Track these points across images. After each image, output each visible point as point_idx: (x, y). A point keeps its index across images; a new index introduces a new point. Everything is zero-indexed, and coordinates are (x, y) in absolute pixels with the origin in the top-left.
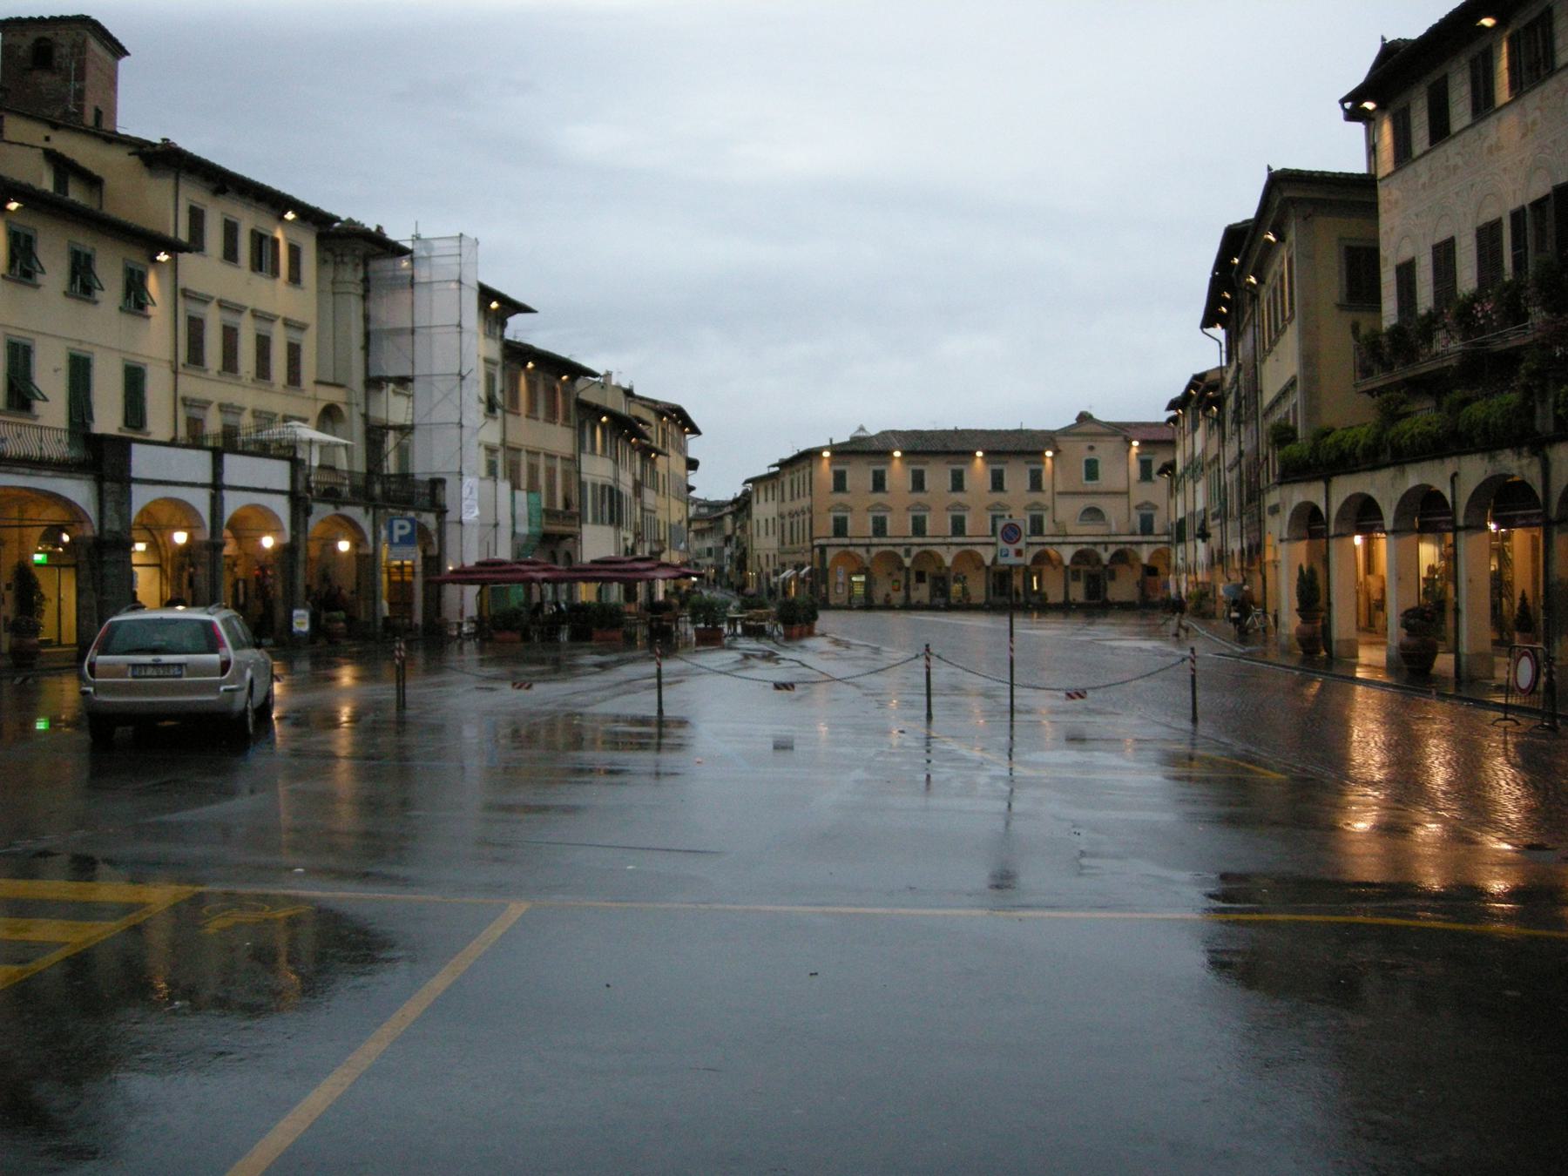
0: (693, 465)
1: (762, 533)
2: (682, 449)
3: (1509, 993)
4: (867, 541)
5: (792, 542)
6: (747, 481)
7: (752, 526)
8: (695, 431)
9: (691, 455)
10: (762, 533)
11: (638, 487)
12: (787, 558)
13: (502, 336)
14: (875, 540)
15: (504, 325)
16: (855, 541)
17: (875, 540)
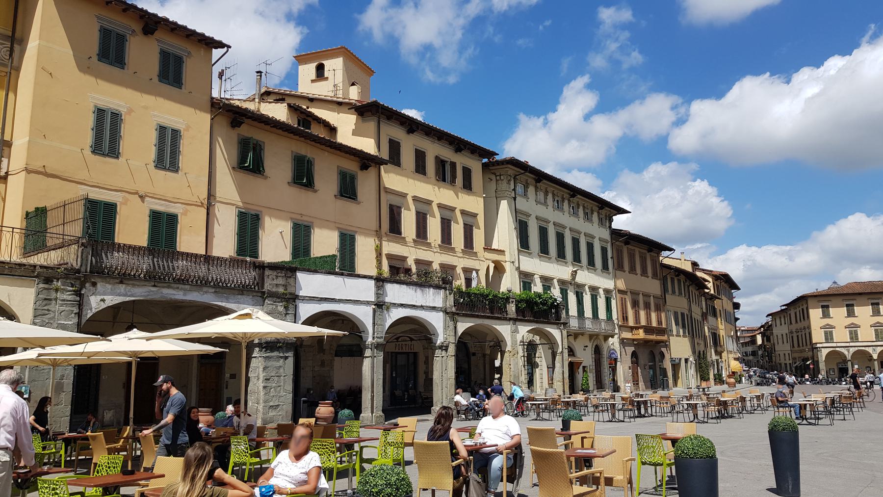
0: (737, 306)
1: (780, 341)
2: (731, 298)
3: (706, 328)
4: (847, 345)
5: (799, 345)
6: (768, 315)
7: (774, 339)
8: (737, 288)
9: (735, 300)
10: (780, 341)
11: (704, 316)
12: (796, 355)
13: (610, 227)
14: (852, 344)
15: (611, 221)
16: (839, 345)
17: (852, 344)
